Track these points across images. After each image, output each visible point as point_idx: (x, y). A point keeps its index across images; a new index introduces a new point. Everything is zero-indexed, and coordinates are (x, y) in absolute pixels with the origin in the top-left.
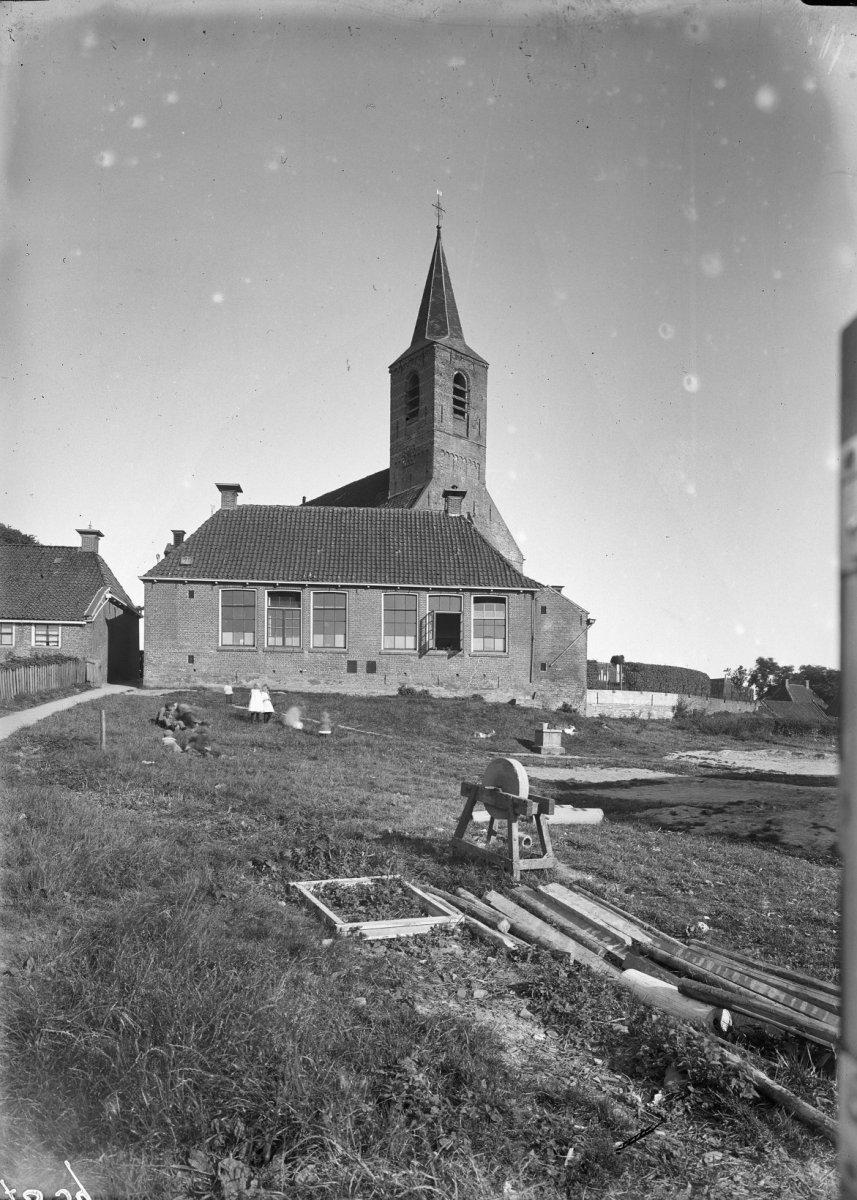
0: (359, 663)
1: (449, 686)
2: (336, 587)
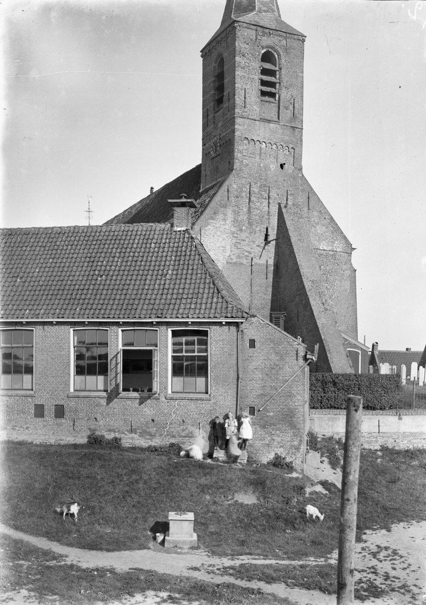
0: (46, 407)
1: (144, 433)
2: (21, 324)
